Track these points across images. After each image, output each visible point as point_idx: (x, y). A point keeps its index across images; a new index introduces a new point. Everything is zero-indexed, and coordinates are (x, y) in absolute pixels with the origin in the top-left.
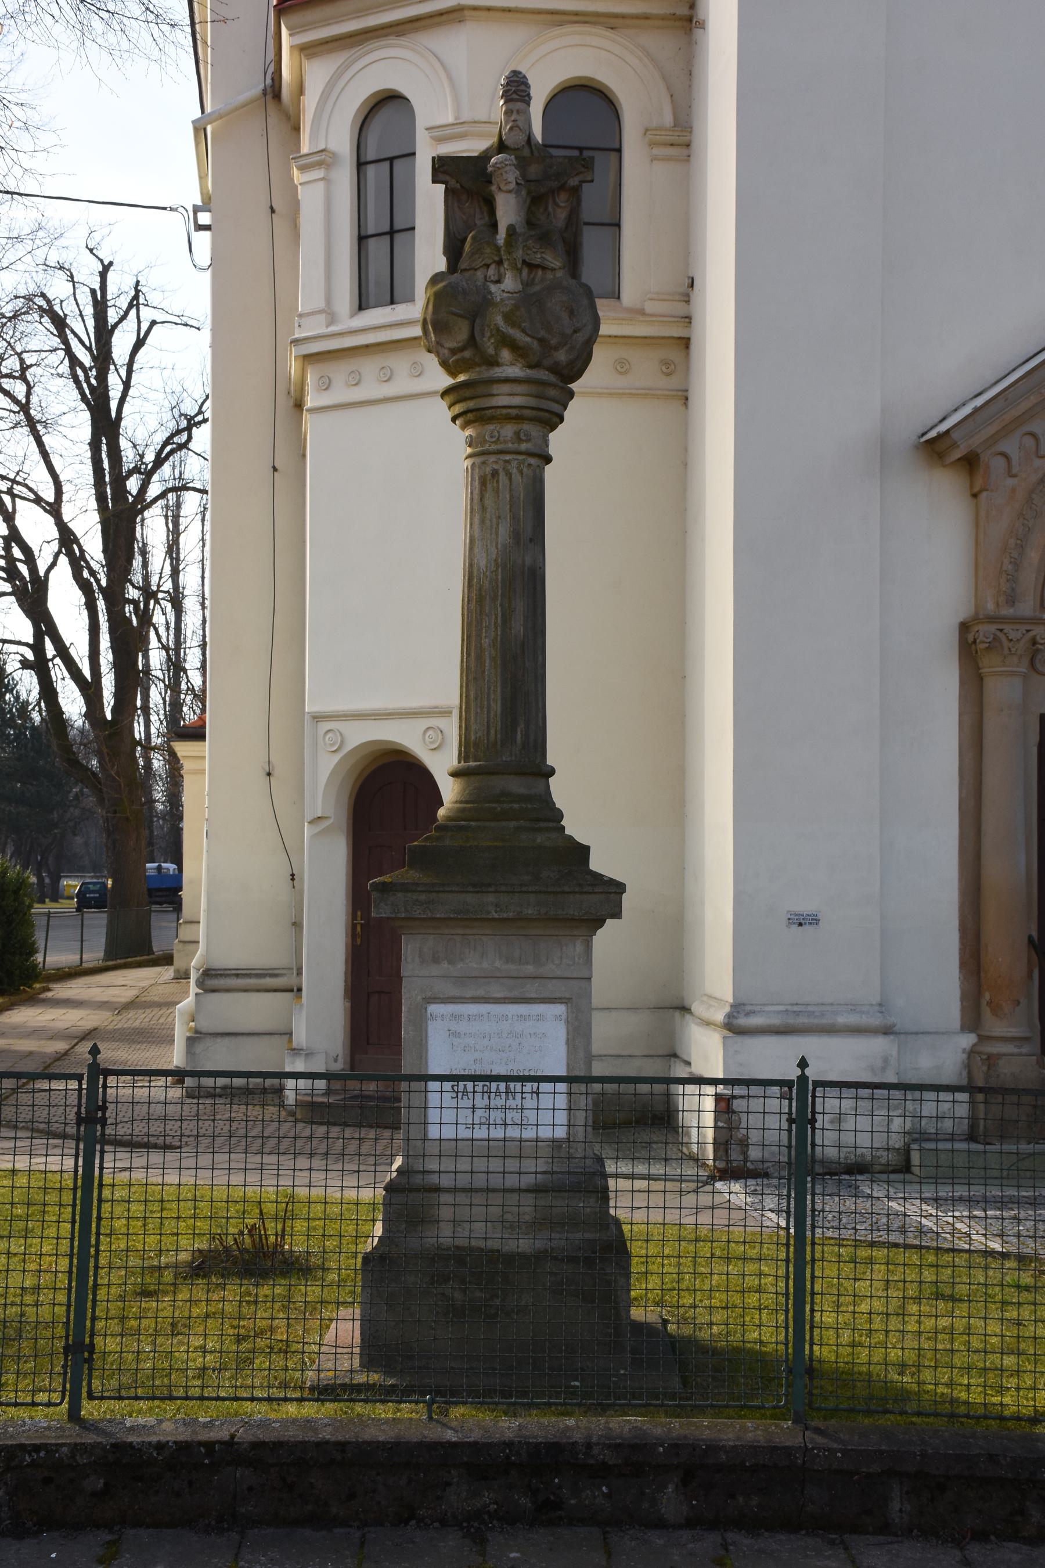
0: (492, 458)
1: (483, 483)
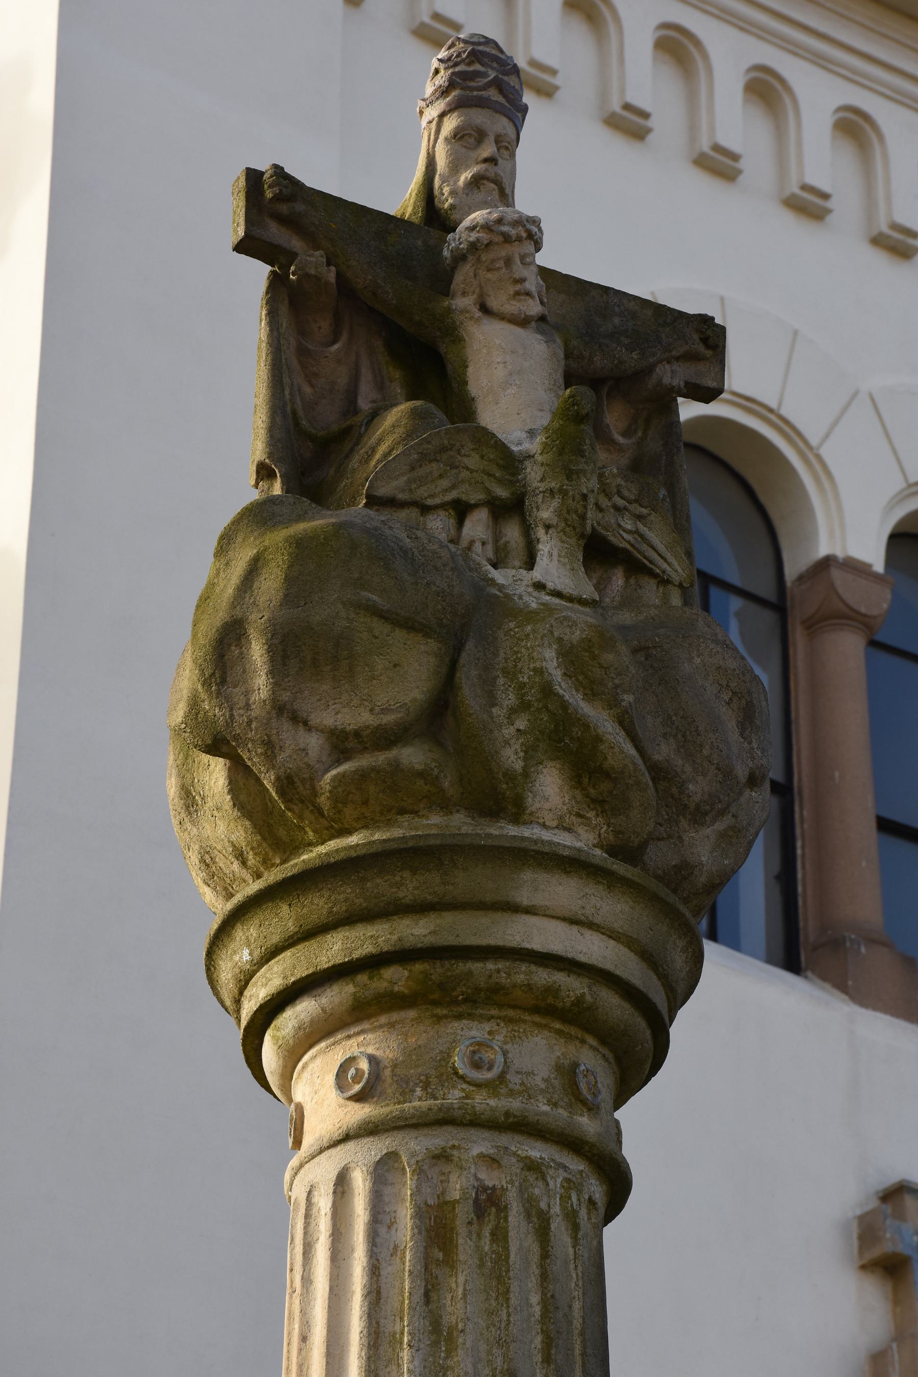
0: (480, 1144)
1: (437, 1231)
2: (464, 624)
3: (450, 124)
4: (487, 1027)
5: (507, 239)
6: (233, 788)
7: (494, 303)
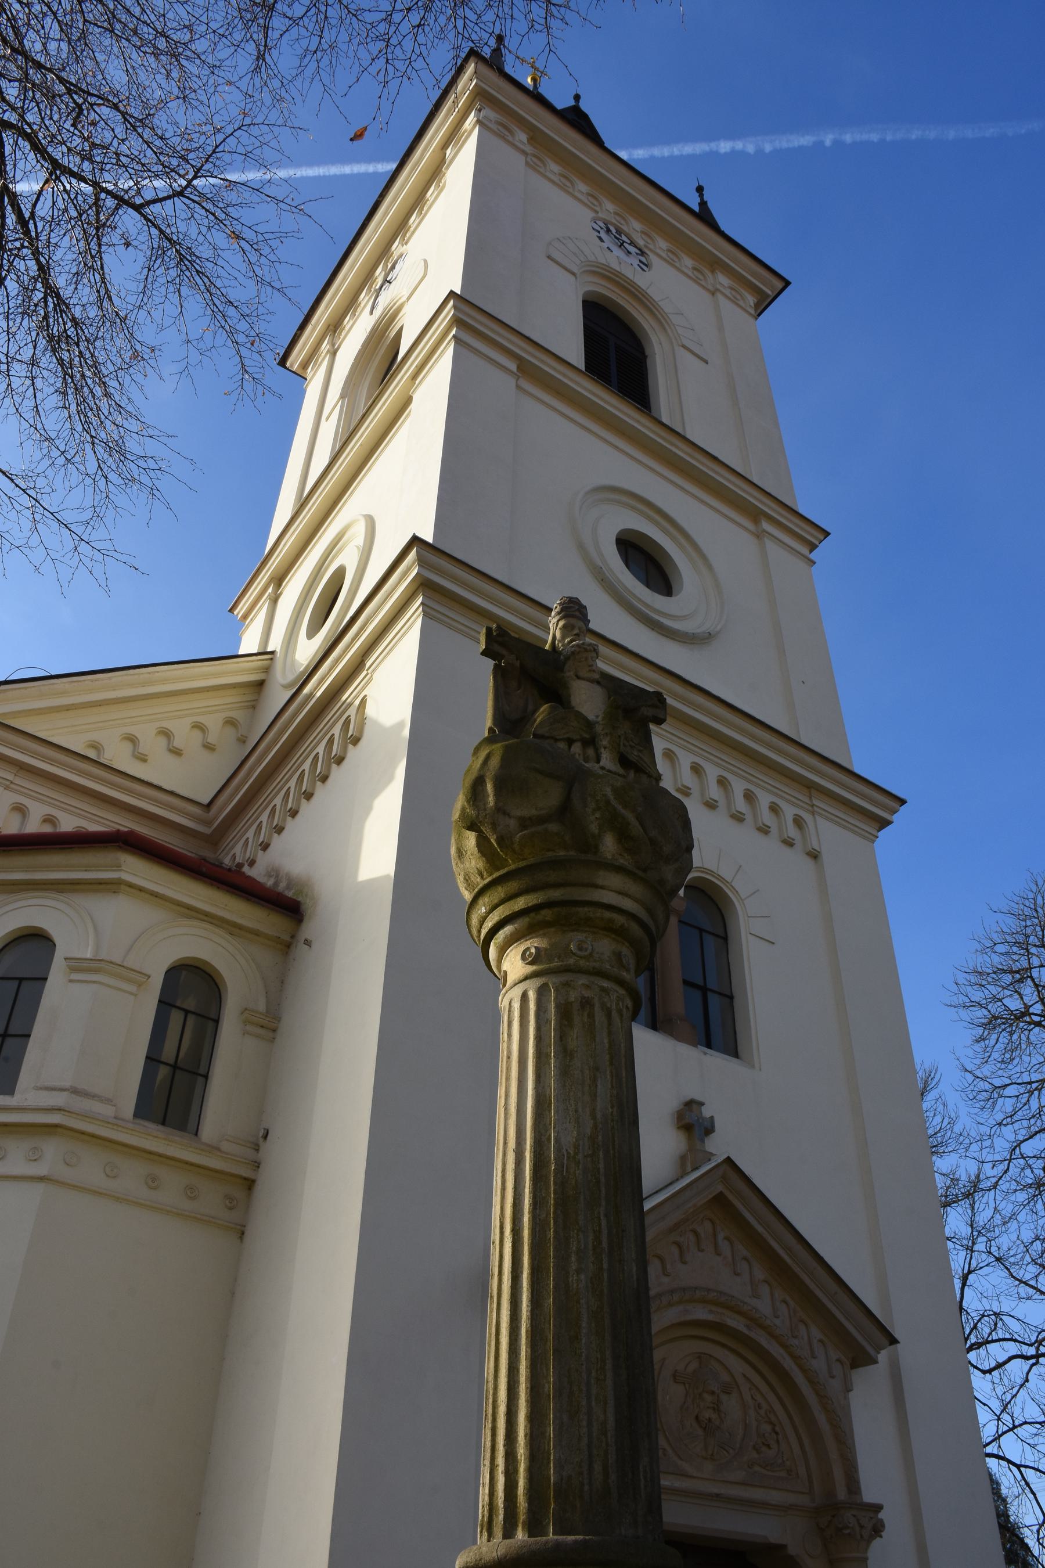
0: (583, 980)
1: (565, 1013)
2: (573, 779)
3: (561, 623)
4: (584, 935)
5: (586, 650)
6: (479, 845)
7: (581, 674)
